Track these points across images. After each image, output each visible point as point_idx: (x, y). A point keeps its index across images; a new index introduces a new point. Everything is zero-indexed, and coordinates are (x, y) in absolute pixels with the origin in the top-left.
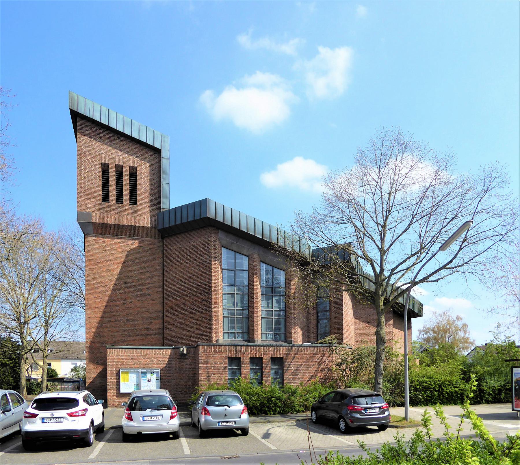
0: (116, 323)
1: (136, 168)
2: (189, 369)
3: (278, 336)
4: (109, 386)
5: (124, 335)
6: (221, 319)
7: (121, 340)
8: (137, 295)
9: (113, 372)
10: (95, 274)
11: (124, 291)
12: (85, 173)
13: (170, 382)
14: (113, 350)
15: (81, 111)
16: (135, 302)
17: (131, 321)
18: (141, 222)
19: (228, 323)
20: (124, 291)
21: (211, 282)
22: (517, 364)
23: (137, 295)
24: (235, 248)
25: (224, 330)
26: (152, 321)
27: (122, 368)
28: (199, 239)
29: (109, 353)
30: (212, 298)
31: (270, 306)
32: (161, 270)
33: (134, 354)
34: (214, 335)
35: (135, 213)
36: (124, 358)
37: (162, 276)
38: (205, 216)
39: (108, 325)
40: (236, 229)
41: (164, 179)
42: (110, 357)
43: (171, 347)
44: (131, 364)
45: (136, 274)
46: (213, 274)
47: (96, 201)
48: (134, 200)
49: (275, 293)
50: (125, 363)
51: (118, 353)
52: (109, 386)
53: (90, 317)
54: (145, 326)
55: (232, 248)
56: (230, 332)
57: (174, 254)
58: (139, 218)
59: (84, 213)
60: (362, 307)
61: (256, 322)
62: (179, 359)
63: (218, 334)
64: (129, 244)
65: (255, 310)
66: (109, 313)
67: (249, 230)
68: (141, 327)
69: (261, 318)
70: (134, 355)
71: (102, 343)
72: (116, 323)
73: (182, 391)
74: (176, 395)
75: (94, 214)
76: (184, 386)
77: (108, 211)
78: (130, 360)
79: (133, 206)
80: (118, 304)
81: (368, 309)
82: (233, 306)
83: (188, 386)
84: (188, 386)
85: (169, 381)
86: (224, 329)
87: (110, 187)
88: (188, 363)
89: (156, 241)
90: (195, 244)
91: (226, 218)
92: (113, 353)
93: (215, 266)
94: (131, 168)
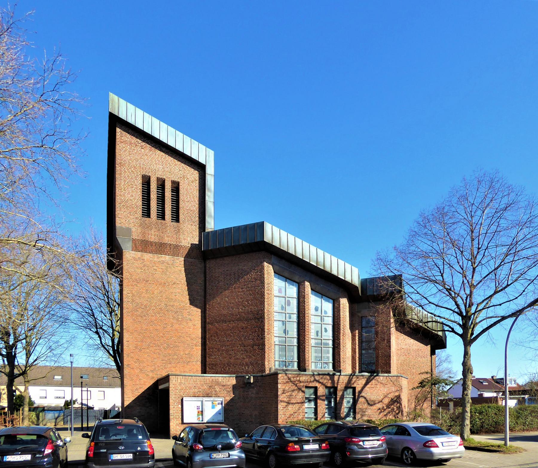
1: (178, 183)
2: (255, 398)
4: (172, 415)
5: (164, 362)
7: (161, 367)
8: (178, 320)
9: (176, 401)
10: (133, 295)
11: (164, 314)
12: (124, 185)
13: (232, 411)
14: (175, 377)
15: (123, 116)
16: (176, 326)
17: (172, 346)
18: (183, 241)
19: (279, 351)
20: (164, 314)
21: (264, 309)
22: (348, 399)
23: (178, 320)
24: (286, 274)
27: (185, 396)
28: (250, 264)
29: (172, 380)
30: (264, 325)
31: (320, 334)
32: (203, 293)
33: (197, 381)
34: (266, 363)
36: (187, 386)
37: (203, 299)
38: (258, 239)
39: (148, 350)
40: (292, 255)
41: (209, 197)
42: (173, 384)
43: (235, 375)
45: (177, 297)
46: (266, 300)
48: (176, 218)
49: (324, 321)
50: (188, 391)
51: (181, 381)
52: (172, 415)
53: (128, 341)
54: (187, 352)
55: (283, 274)
56: (281, 360)
57: (219, 277)
58: (181, 236)
59: (124, 227)
61: (307, 350)
62: (243, 387)
63: (271, 362)
64: (169, 264)
65: (307, 338)
66: (149, 337)
67: (304, 257)
68: (182, 353)
70: (197, 383)
71: (141, 370)
73: (247, 421)
74: (239, 425)
75: (134, 229)
76: (250, 415)
77: (149, 227)
78: (193, 388)
79: (175, 224)
81: (408, 340)
83: (254, 415)
84: (254, 415)
85: (232, 410)
87: (151, 202)
88: (254, 392)
89: (197, 262)
90: (245, 267)
91: (282, 244)
92: (176, 380)
93: (268, 292)
94: (173, 182)
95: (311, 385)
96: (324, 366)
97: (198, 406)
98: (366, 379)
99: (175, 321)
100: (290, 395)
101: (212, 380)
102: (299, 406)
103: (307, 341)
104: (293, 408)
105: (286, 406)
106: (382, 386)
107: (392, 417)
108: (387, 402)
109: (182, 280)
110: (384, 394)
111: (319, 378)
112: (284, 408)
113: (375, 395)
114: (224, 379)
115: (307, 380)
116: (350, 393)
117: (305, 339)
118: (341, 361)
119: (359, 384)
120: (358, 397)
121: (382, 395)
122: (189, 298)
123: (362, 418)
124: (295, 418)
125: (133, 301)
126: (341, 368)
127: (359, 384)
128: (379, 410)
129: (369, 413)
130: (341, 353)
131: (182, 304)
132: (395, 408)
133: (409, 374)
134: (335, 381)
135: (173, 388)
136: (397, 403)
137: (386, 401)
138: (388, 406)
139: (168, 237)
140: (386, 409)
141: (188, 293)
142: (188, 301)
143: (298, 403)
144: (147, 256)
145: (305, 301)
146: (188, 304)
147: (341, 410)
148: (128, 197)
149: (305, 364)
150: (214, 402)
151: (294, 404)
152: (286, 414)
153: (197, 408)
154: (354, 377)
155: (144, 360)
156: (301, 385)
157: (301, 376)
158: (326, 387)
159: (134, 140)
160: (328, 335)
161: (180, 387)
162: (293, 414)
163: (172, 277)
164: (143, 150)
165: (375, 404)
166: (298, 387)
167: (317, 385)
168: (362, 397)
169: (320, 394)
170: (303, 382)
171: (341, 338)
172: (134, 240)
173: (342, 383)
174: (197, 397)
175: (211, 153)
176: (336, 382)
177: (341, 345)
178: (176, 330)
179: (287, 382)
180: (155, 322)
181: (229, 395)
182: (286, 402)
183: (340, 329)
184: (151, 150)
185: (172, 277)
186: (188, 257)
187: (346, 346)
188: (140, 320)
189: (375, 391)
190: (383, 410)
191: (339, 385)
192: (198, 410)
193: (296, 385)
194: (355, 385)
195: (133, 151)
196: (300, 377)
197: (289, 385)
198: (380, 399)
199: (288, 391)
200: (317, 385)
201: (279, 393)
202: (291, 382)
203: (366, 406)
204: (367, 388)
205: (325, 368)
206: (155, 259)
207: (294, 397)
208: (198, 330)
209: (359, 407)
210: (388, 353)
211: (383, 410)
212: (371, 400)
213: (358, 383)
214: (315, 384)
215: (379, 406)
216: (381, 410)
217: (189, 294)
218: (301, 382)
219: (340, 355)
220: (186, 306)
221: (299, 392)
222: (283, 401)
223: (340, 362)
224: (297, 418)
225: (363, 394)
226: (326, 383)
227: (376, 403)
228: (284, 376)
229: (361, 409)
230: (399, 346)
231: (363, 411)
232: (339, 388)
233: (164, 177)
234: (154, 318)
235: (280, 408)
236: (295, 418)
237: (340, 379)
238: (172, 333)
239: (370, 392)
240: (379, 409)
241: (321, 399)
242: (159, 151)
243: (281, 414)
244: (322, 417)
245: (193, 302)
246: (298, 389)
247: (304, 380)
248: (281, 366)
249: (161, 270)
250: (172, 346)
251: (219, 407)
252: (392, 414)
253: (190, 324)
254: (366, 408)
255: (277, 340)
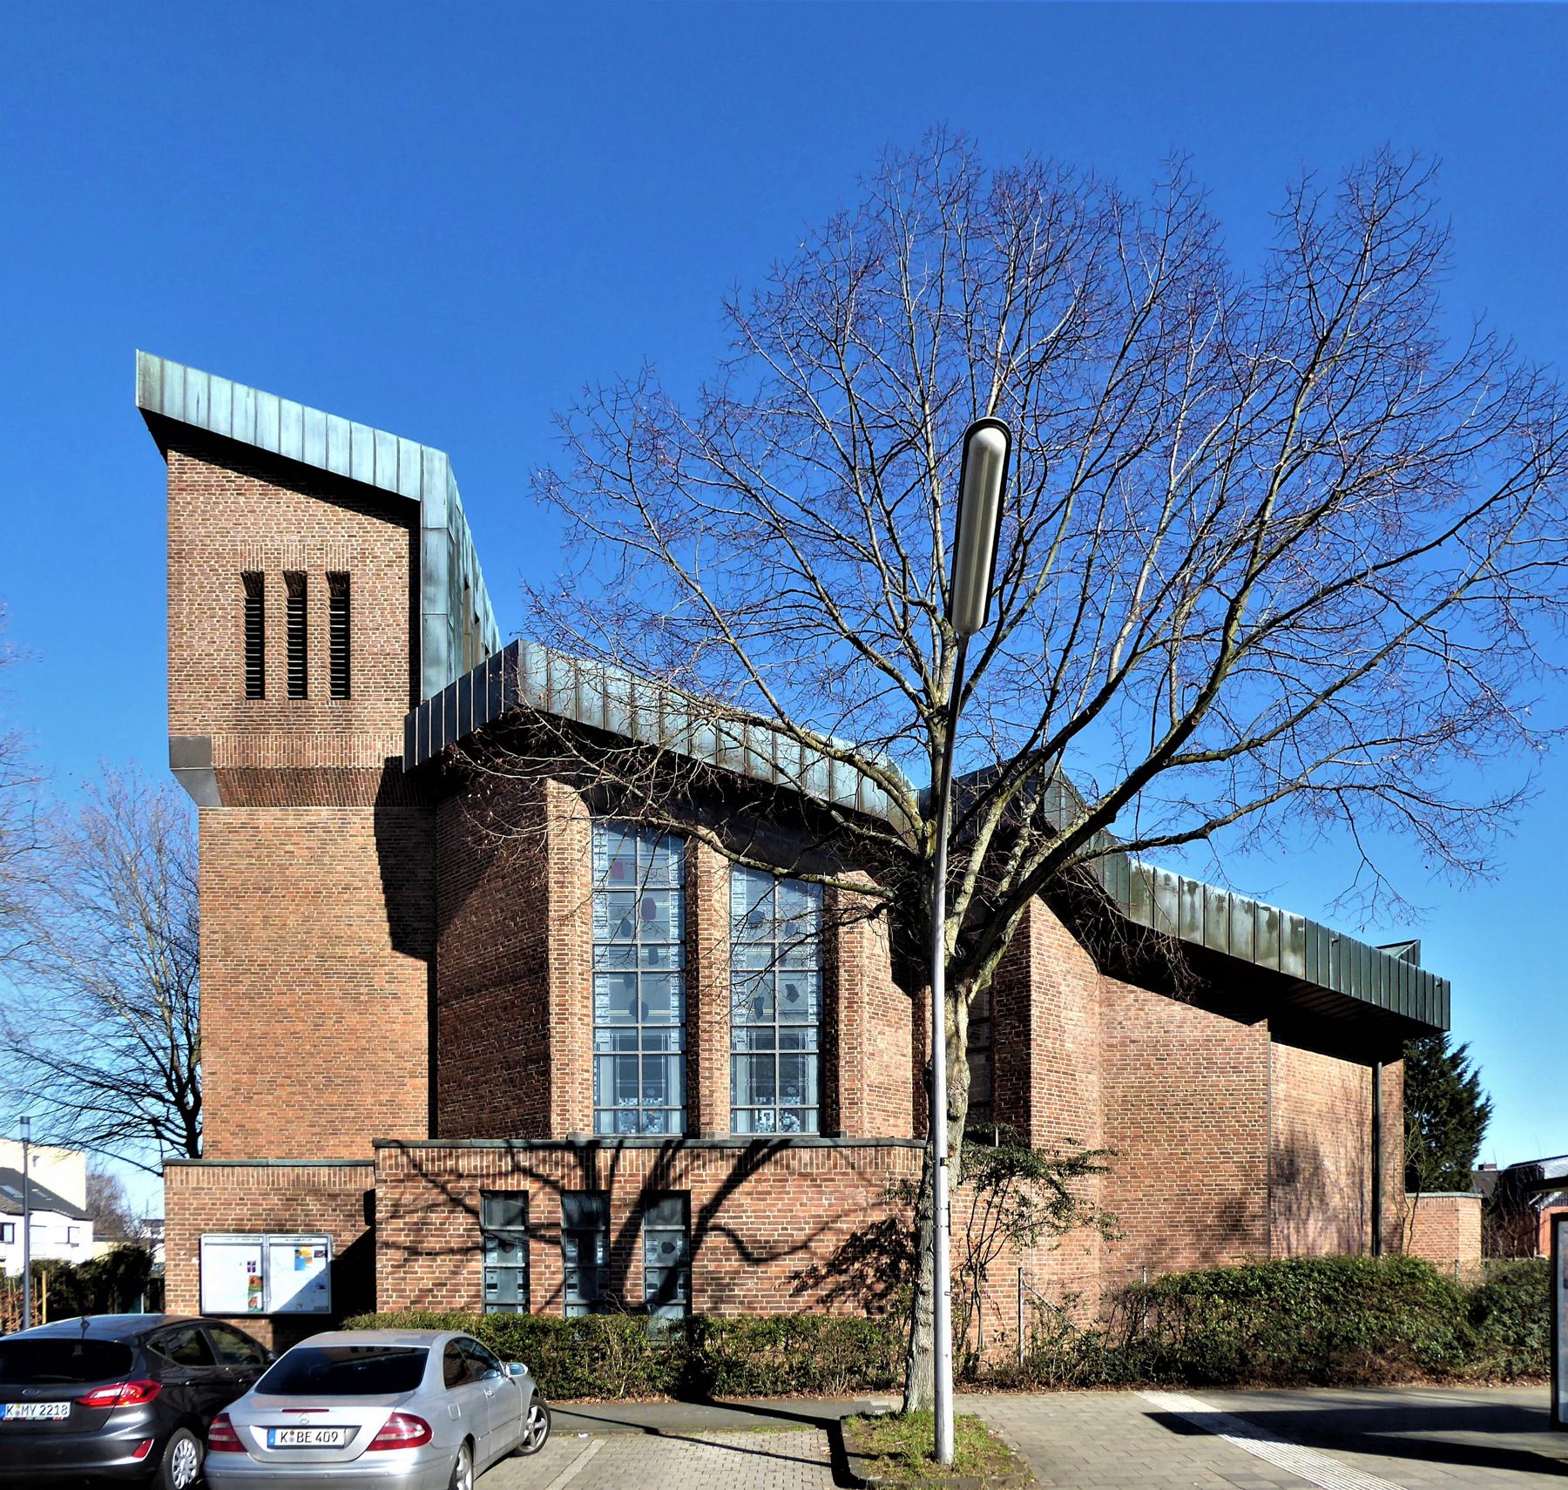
0: (294, 1089)
3: (794, 1118)
5: (317, 1130)
6: (584, 1062)
8: (356, 999)
10: (228, 936)
11: (317, 984)
12: (191, 613)
15: (173, 411)
16: (352, 1019)
17: (339, 1081)
20: (317, 984)
23: (356, 999)
25: (734, 1102)
26: (406, 1080)
31: (767, 1011)
35: (345, 726)
39: (270, 1098)
44: (759, 1217)
45: (354, 928)
47: (225, 699)
48: (342, 687)
54: (384, 1098)
60: (1136, 1001)
61: (707, 1069)
68: (370, 1100)
69: (727, 1056)
72: (294, 1089)
75: (217, 741)
77: (260, 728)
80: (300, 1027)
82: (634, 1018)
86: (735, 1096)
95: (501, 1185)
96: (787, 1121)
97: (252, 1260)
98: (733, 1162)
99: (349, 1005)
100: (423, 1224)
101: (298, 1176)
102: (457, 1261)
103: (705, 1036)
104: (431, 1267)
105: (405, 1260)
106: (808, 1186)
107: (855, 1308)
108: (832, 1249)
109: (370, 877)
110: (820, 1216)
111: (534, 1162)
112: (399, 1266)
113: (776, 1223)
114: (335, 1174)
115: (488, 1167)
116: (673, 1214)
117: (698, 1028)
118: (842, 1100)
119: (703, 1182)
120: (697, 1230)
121: (808, 1223)
122: (391, 928)
123: (716, 1308)
124: (441, 1303)
125: (227, 953)
126: (842, 1126)
127: (703, 1182)
128: (794, 1278)
129: (749, 1290)
130: (842, 1072)
131: (370, 950)
132: (871, 1272)
133: (1162, 1137)
134: (600, 1171)
135: (175, 1204)
136: (880, 1254)
137: (828, 1245)
138: (834, 1267)
139: (315, 748)
140: (829, 1274)
141: (389, 913)
142: (386, 939)
143: (452, 1251)
144: (267, 816)
145: (697, 898)
146: (389, 949)
147: (626, 1278)
148: (201, 646)
149: (699, 1116)
150: (302, 1249)
151: (437, 1254)
152: (404, 1290)
153: (246, 1267)
154: (683, 1152)
155: (258, 1126)
156: (463, 1188)
157: (463, 1155)
158: (563, 1192)
159: (218, 474)
160: (801, 1009)
161: (195, 1202)
162: (431, 1290)
163: (339, 868)
164: (242, 499)
165: (774, 1257)
166: (448, 1194)
167: (527, 1185)
168: (717, 1228)
169: (540, 1218)
170: (468, 1176)
171: (843, 1015)
172: (219, 772)
173: (631, 1175)
174: (250, 1231)
175: (438, 459)
176: (603, 1173)
177: (842, 1044)
178: (353, 1031)
179: (409, 1177)
180: (291, 1011)
181: (354, 1226)
182: (405, 1248)
183: (837, 986)
184: (266, 495)
185: (339, 868)
186: (384, 800)
187: (861, 1044)
188: (246, 1009)
189: (774, 1205)
190: (811, 1282)
191: (616, 1185)
192: (252, 1274)
193: (444, 1190)
194: (686, 1185)
195: (213, 510)
196: (457, 1157)
197: (418, 1188)
198: (800, 1236)
199: (412, 1208)
200: (527, 1185)
201: (378, 1215)
202: (425, 1175)
203: (734, 1263)
204: (738, 1195)
205: (788, 1127)
206: (290, 822)
207: (436, 1230)
208: (420, 1026)
209: (706, 1266)
210: (1022, 1059)
211: (811, 1282)
212: (760, 1242)
213: (701, 1175)
214: (519, 1181)
215: (797, 1263)
216: (803, 1281)
217: (390, 919)
218: (460, 1176)
219: (837, 1079)
220: (381, 954)
221: (451, 1212)
222: (393, 1243)
223: (837, 1103)
224: (450, 1303)
225: (722, 1218)
226: (563, 1178)
227: (780, 1254)
228: (396, 1157)
229: (715, 1279)
230: (1118, 1033)
231: (721, 1289)
232: (617, 1194)
233: (262, 568)
234: (286, 1000)
235: (384, 1266)
236: (441, 1303)
237: (622, 1163)
238: (340, 1041)
239: (754, 1211)
240: (797, 1275)
241: (542, 1239)
242: (288, 492)
243: (387, 1290)
244: (548, 1303)
245: (402, 941)
246: (452, 1200)
247: (475, 1168)
248: (621, 1128)
249: (306, 853)
250: (339, 1081)
251: (318, 1266)
252: (855, 1295)
253: (395, 1010)
254: (737, 1272)
255: (608, 1040)
